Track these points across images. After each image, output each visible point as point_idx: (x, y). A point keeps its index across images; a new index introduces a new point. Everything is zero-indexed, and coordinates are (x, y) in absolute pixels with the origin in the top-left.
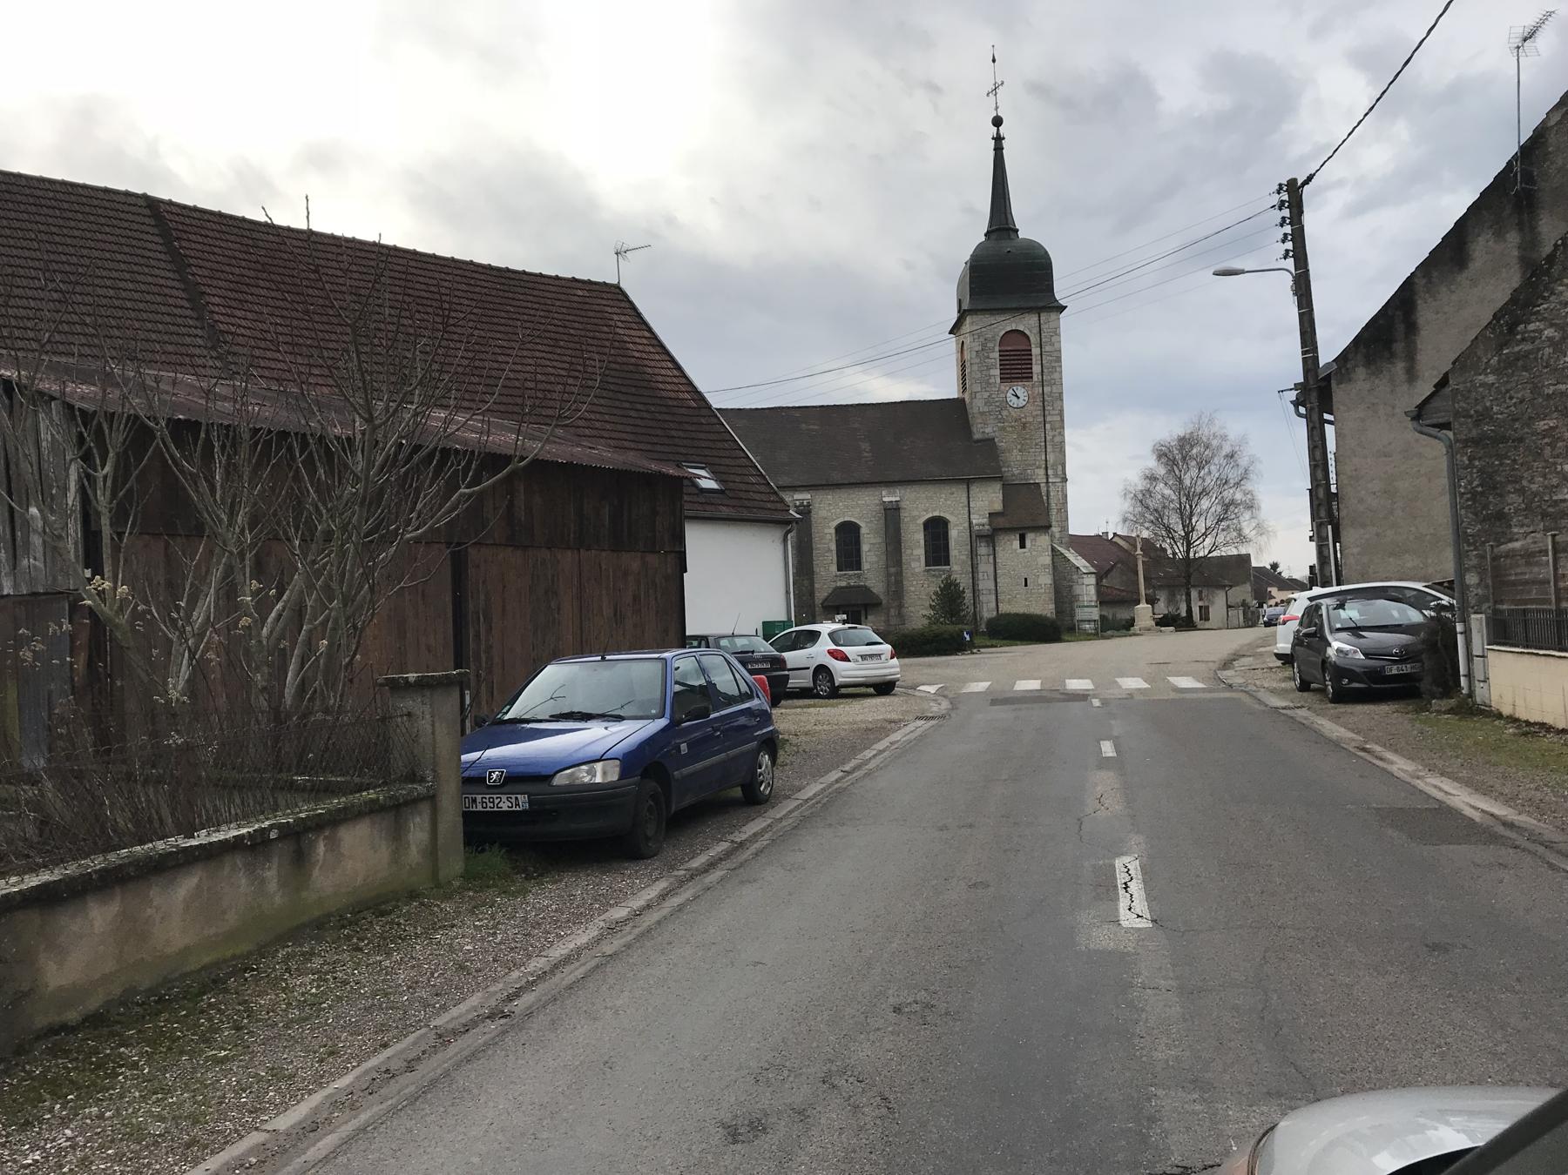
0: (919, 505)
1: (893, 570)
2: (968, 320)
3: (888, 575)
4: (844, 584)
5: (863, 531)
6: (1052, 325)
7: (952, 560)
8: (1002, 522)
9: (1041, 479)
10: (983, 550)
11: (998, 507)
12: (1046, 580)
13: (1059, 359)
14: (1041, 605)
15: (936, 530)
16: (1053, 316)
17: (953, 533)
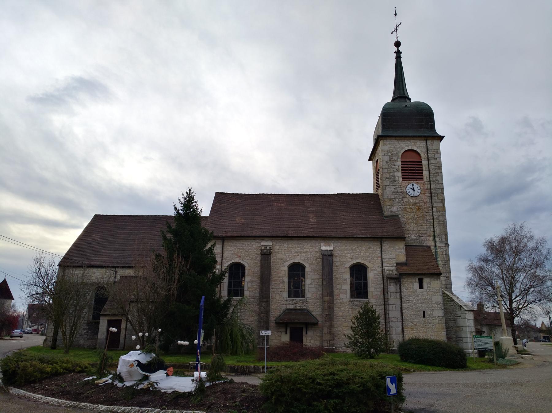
0: (347, 254)
1: (327, 299)
2: (381, 143)
3: (323, 302)
4: (292, 307)
5: (307, 270)
6: (435, 147)
7: (370, 295)
8: (405, 269)
9: (431, 243)
10: (392, 288)
11: (403, 259)
12: (439, 313)
13: (440, 168)
14: (436, 333)
15: (359, 272)
16: (435, 142)
17: (371, 275)
